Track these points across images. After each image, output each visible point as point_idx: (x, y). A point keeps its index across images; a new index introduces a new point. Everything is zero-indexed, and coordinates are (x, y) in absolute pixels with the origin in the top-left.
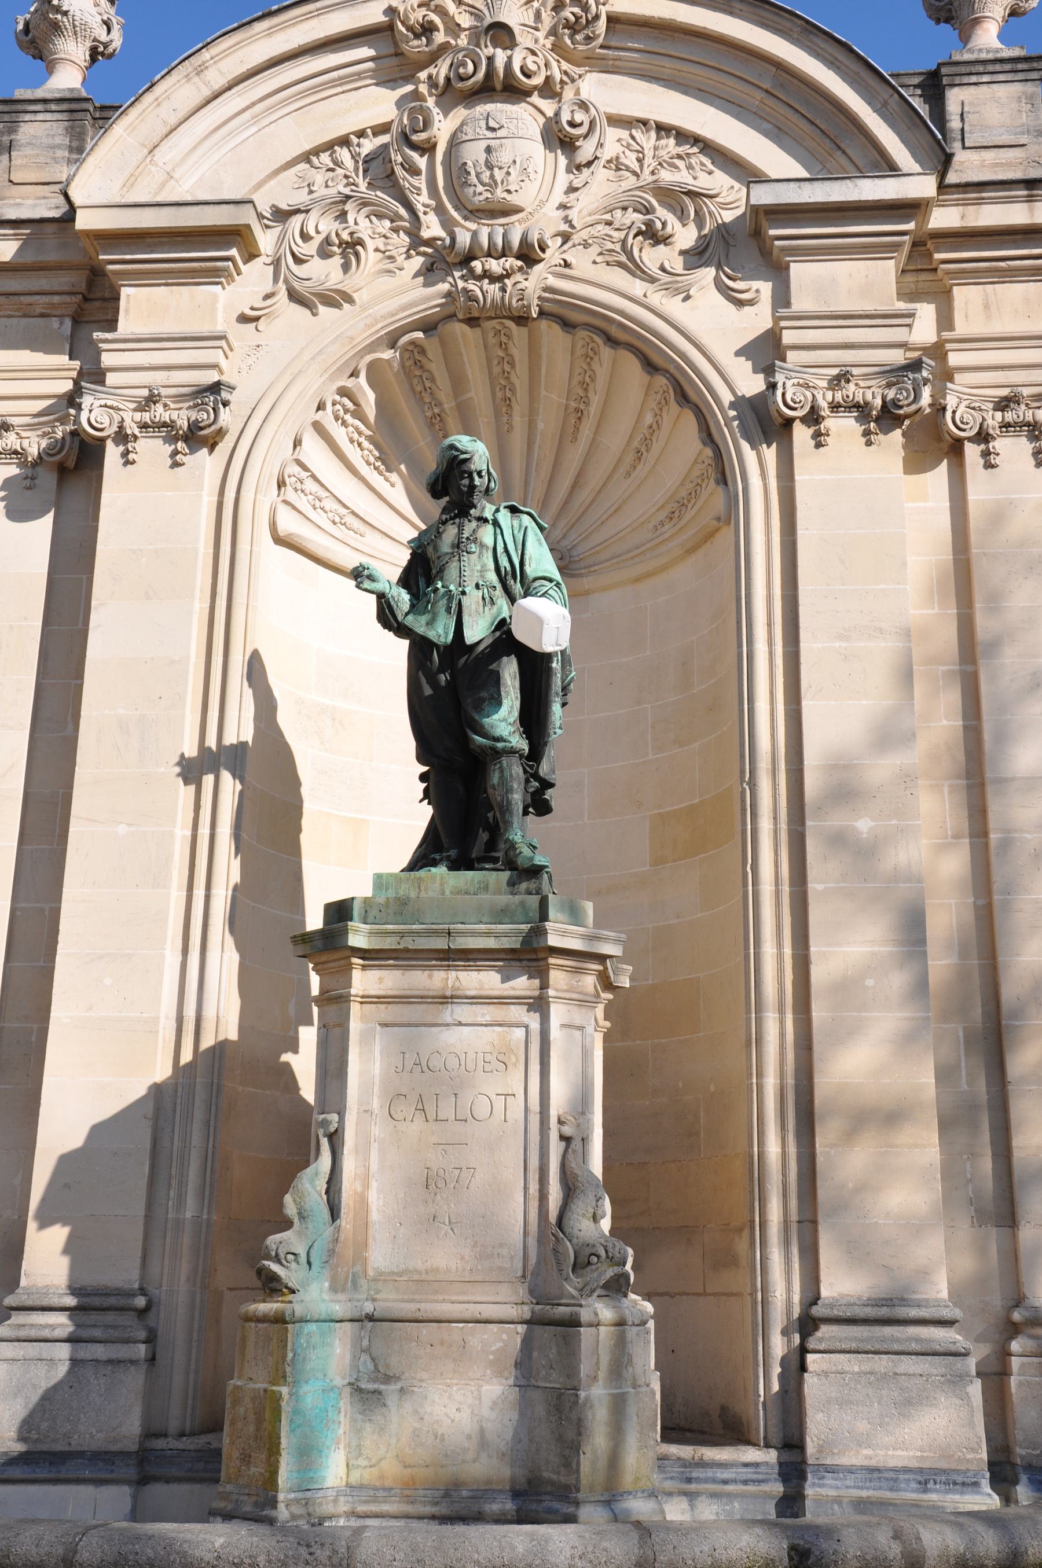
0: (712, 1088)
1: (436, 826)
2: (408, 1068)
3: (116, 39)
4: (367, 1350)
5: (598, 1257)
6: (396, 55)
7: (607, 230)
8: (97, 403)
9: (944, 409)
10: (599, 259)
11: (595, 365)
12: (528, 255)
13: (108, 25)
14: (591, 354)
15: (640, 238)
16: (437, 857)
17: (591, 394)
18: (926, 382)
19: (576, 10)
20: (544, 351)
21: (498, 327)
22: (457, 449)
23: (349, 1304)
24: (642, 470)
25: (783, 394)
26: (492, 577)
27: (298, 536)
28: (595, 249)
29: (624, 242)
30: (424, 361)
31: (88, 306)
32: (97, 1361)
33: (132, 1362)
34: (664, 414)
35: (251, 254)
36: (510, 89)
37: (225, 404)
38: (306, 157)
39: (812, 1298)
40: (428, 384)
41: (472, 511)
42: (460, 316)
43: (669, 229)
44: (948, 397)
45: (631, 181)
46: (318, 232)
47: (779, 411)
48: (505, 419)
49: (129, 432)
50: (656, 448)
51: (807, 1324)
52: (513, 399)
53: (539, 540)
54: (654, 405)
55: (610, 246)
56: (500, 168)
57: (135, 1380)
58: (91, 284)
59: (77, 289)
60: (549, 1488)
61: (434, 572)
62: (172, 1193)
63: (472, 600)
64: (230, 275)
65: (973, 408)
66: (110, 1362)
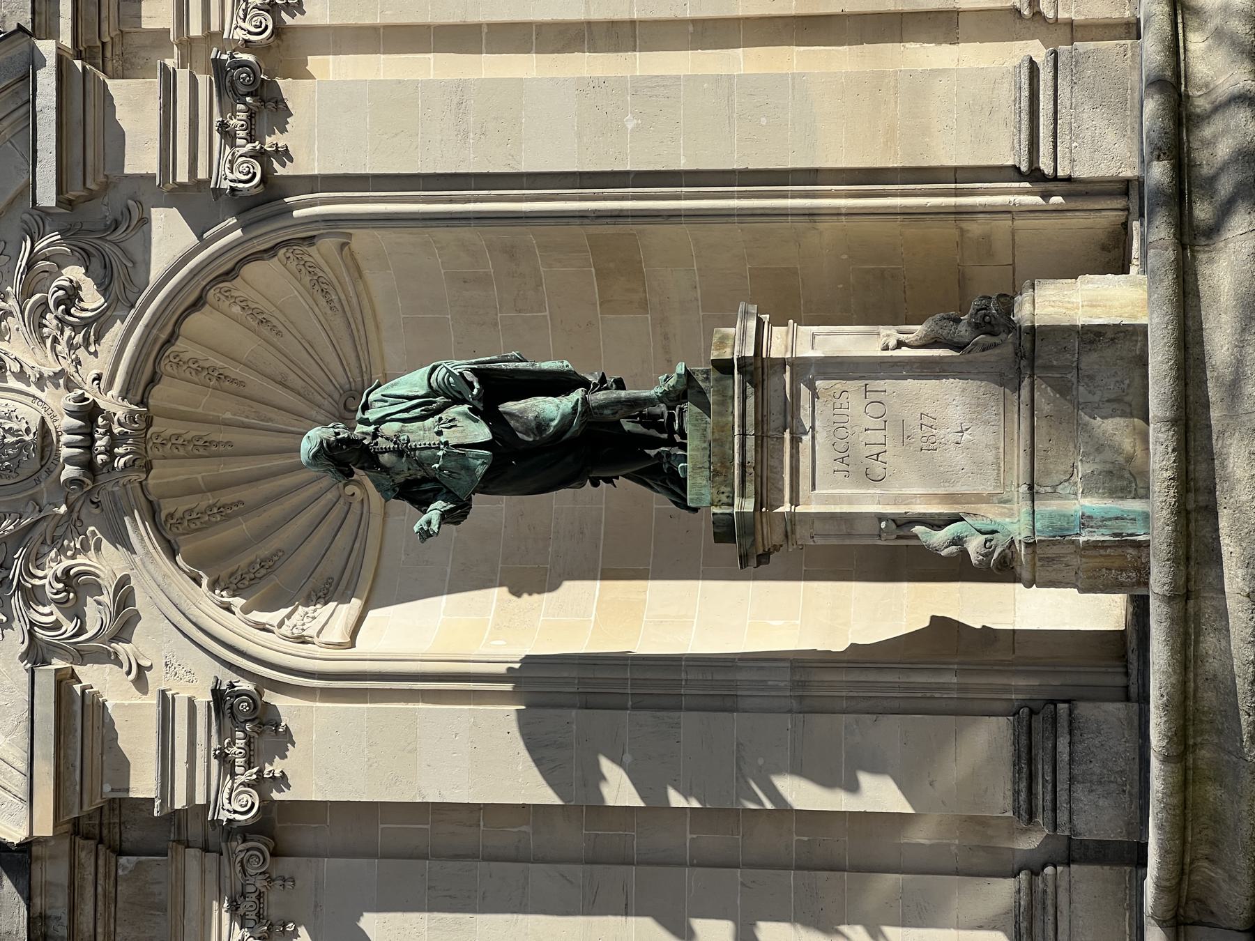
0: (845, 257)
1: (635, 472)
2: (844, 467)
4: (1054, 487)
5: (985, 315)
7: (63, 341)
8: (227, 806)
9: (246, 41)
10: (92, 349)
11: (186, 357)
12: (89, 413)
15: (73, 311)
18: (232, 57)
25: (240, 181)
26: (430, 422)
28: (81, 353)
30: (177, 515)
31: (106, 841)
35: (74, 677)
37: (232, 686)
40: (194, 516)
43: (67, 284)
44: (236, 37)
46: (51, 614)
47: (256, 186)
48: (222, 448)
49: (254, 777)
50: (263, 304)
51: (1034, 175)
52: (205, 439)
53: (392, 386)
56: (4, 437)
57: (1083, 709)
59: (94, 847)
62: (937, 695)
63: (452, 437)
65: (245, 16)
66: (1071, 733)
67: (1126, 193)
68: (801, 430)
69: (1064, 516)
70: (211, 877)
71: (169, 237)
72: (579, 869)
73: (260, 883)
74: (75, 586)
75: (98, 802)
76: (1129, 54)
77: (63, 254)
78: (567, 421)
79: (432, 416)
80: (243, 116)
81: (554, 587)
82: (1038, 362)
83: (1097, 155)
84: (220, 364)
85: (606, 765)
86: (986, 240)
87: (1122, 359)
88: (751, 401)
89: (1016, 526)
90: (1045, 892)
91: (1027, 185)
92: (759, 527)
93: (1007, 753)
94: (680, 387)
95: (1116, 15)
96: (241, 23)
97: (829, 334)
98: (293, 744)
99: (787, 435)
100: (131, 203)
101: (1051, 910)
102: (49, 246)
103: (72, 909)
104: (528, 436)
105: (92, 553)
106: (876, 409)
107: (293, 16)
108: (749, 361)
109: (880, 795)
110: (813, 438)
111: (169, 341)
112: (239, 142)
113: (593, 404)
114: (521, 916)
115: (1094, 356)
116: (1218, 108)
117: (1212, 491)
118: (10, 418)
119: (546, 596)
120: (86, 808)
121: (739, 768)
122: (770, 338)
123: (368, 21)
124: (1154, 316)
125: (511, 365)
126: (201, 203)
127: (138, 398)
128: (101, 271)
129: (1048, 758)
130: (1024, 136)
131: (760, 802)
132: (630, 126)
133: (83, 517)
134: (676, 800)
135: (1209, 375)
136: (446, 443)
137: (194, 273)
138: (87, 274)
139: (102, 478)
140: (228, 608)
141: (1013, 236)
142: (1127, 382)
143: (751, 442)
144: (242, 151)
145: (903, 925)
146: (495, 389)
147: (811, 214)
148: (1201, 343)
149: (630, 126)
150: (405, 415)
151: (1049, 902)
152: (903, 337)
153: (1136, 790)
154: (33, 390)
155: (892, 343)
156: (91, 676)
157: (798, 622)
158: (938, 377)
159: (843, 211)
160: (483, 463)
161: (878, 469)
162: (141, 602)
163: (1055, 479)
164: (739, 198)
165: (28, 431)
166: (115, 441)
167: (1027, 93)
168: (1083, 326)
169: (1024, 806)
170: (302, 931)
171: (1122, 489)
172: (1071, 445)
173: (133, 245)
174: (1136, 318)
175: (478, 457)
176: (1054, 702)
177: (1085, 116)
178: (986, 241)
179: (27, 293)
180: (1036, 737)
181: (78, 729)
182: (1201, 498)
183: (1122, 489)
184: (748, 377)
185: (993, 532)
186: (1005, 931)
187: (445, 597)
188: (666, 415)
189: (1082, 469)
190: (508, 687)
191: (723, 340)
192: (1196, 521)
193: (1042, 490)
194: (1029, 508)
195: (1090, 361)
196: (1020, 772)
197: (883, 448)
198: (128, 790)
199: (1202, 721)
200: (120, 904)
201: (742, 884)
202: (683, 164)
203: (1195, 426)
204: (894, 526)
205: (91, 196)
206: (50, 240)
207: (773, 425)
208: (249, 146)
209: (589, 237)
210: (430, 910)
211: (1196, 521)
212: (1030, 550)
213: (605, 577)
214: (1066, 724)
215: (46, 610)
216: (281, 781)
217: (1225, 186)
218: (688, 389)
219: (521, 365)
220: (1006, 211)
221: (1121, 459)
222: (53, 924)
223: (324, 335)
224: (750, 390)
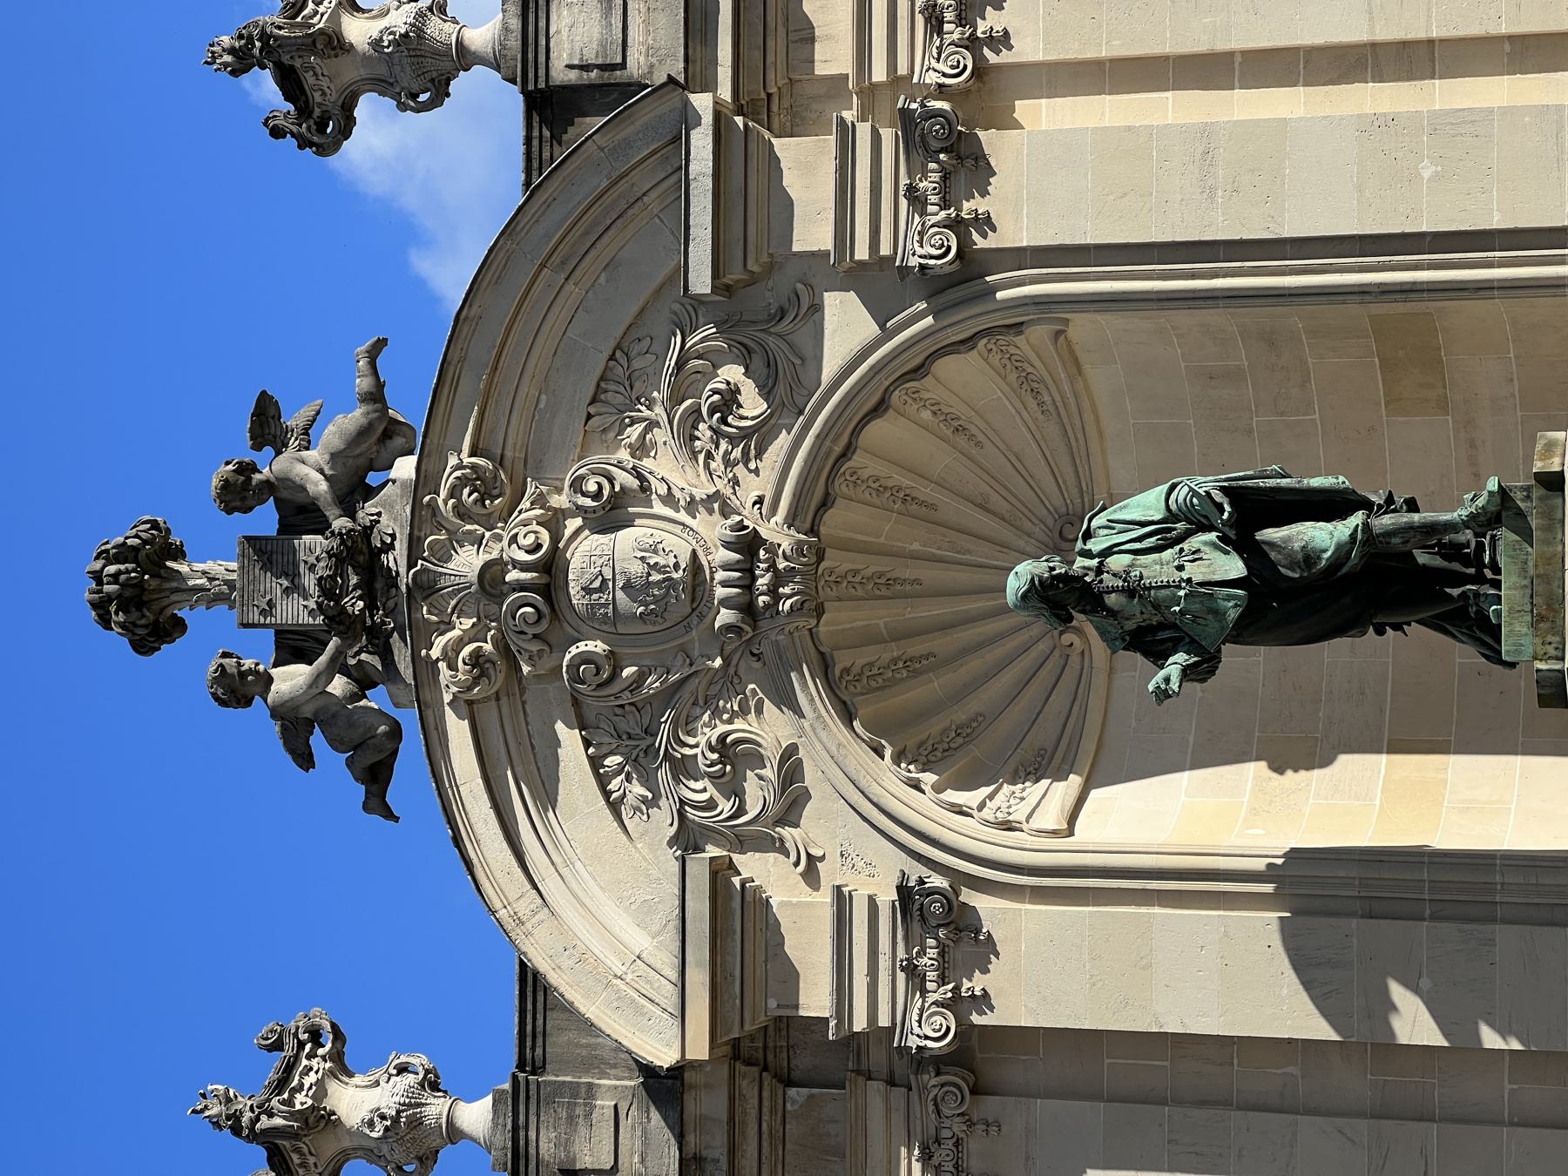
3: (419, 1060)
6: (498, 699)
8: (917, 1030)
9: (940, 86)
10: (752, 466)
12: (748, 545)
13: (402, 1069)
15: (730, 419)
17: (890, 483)
19: (466, 491)
25: (932, 257)
26: (1168, 554)
27: (1063, 806)
28: (740, 470)
31: (771, 1065)
36: (551, 567)
37: (921, 882)
38: (615, 807)
40: (875, 671)
43: (723, 386)
46: (705, 790)
47: (951, 263)
48: (908, 587)
56: (649, 574)
59: (757, 1075)
63: (1195, 572)
65: (939, 54)
70: (898, 1118)
71: (846, 326)
72: (1363, 1125)
73: (958, 1127)
74: (734, 758)
77: (719, 350)
78: (1343, 551)
80: (935, 177)
81: (1326, 762)
85: (1398, 992)
94: (1492, 508)
96: (934, 64)
98: (997, 955)
100: (800, 286)
102: (702, 340)
104: (1293, 571)
105: (752, 717)
107: (998, 52)
112: (930, 209)
113: (1376, 530)
118: (655, 552)
119: (1316, 772)
120: (747, 1027)
123: (1090, 54)
125: (1271, 483)
126: (882, 284)
127: (807, 525)
132: (1426, 174)
133: (741, 672)
134: (1491, 1039)
136: (1189, 581)
137: (876, 370)
139: (764, 625)
140: (916, 785)
144: (934, 219)
146: (1249, 512)
149: (1426, 174)
150: (1137, 546)
154: (682, 516)
160: (1236, 605)
165: (676, 566)
166: (779, 579)
173: (802, 338)
175: (1229, 598)
179: (675, 399)
187: (1187, 773)
188: (1473, 545)
190: (1268, 888)
198: (797, 1007)
200: (788, 1146)
202: (1497, 221)
205: (753, 280)
206: (704, 335)
208: (943, 214)
213: (1393, 749)
215: (699, 785)
216: (983, 1001)
219: (1284, 482)
223: (1034, 446)
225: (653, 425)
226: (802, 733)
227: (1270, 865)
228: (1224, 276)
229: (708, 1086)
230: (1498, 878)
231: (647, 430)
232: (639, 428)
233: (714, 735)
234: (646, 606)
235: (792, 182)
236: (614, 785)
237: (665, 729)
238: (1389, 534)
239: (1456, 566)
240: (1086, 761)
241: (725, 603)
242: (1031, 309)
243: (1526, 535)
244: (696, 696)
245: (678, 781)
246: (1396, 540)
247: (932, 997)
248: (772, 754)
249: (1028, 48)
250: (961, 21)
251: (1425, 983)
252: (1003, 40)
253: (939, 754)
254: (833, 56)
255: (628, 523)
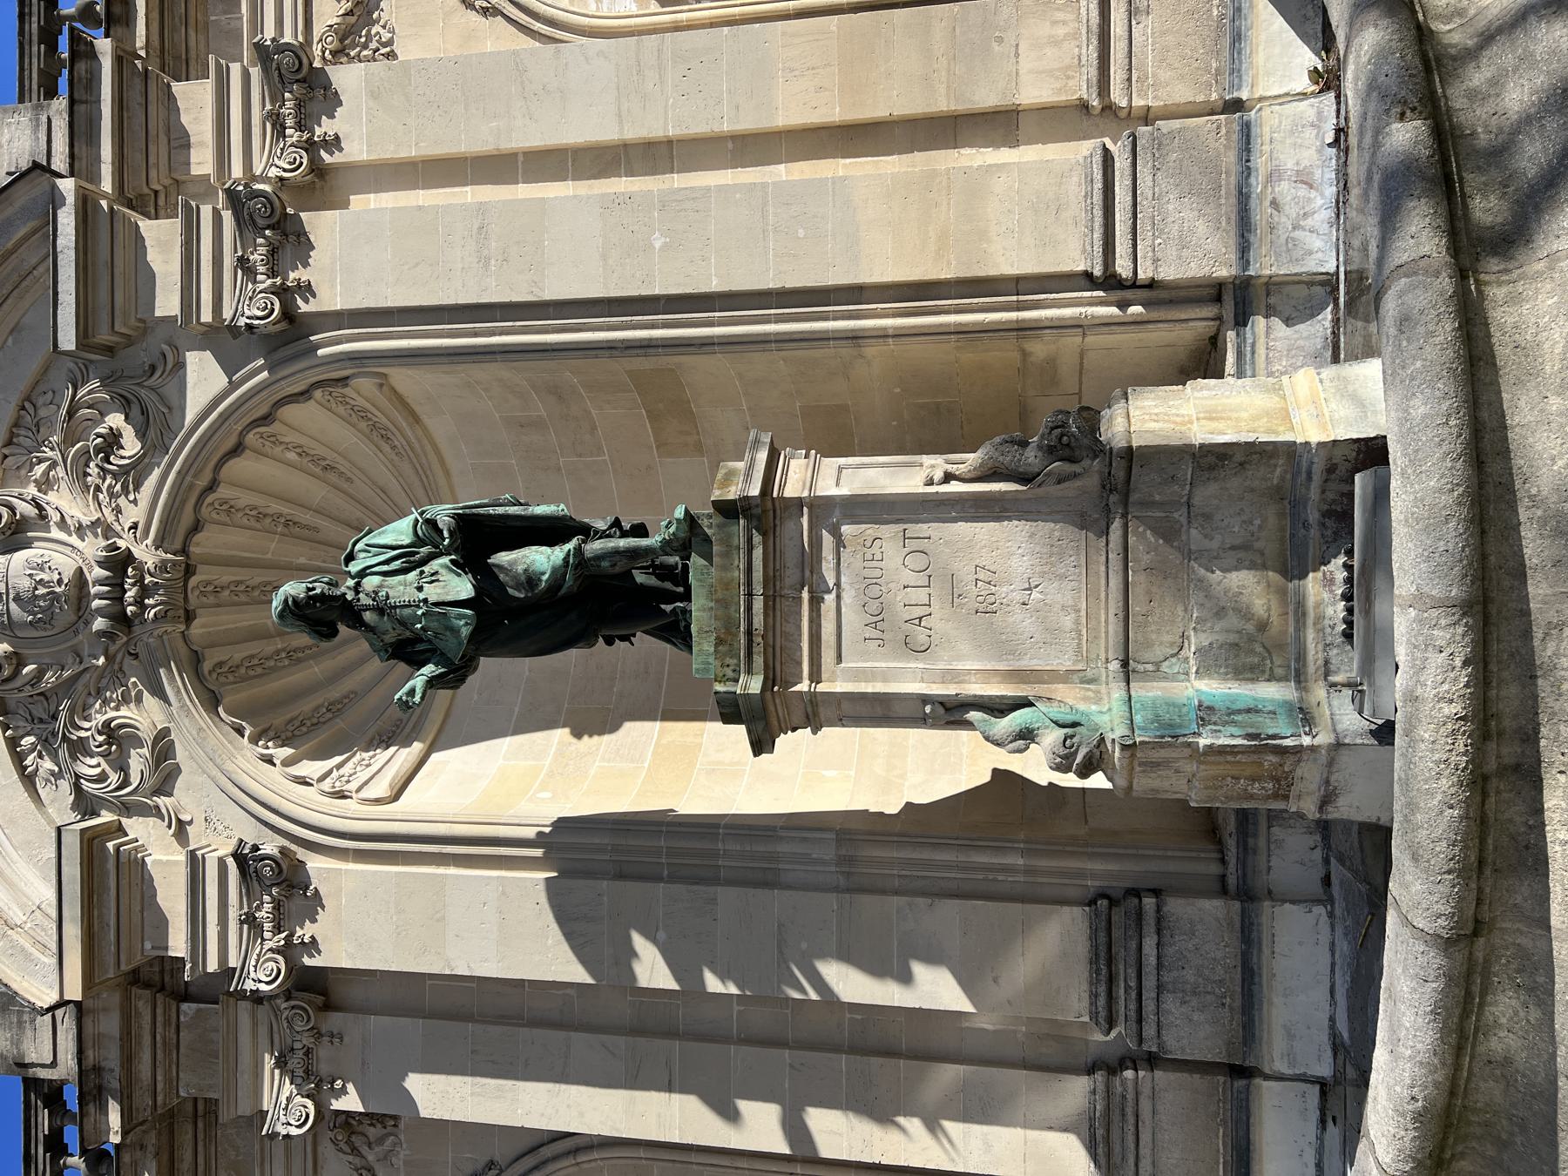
4: (1158, 664)
5: (1062, 435)
9: (281, 179)
10: (131, 497)
12: (119, 563)
14: (225, 507)
16: (683, 624)
17: (269, 511)
20: (224, 552)
21: (197, 593)
22: (283, 611)
23: (1112, 685)
24: (343, 466)
26: (413, 575)
28: (122, 501)
29: (115, 476)
31: (168, 987)
32: (1158, 944)
33: (1158, 910)
34: (286, 440)
37: (255, 848)
38: (28, 780)
39: (1088, 281)
40: (256, 661)
41: (349, 597)
42: (183, 627)
45: (60, 471)
50: (321, 451)
51: (1110, 282)
54: (278, 449)
55: (118, 487)
57: (1176, 906)
58: (147, 985)
60: (1289, 476)
61: (408, 634)
63: (433, 593)
64: (136, 849)
66: (1159, 932)
67: (1218, 299)
68: (823, 587)
69: (1174, 705)
70: (263, 1031)
71: (203, 379)
72: (621, 1041)
73: (307, 1040)
74: (117, 739)
75: (138, 960)
76: (1223, 131)
77: (104, 401)
79: (414, 569)
80: (263, 250)
81: (614, 728)
82: (1134, 497)
83: (1185, 253)
84: (286, 511)
85: (639, 942)
86: (1051, 363)
87: (1252, 490)
88: (758, 553)
89: (1106, 718)
90: (1124, 1097)
91: (1101, 293)
92: (772, 708)
93: (1082, 948)
95: (1201, 98)
96: (277, 161)
97: (859, 467)
98: (323, 908)
99: (805, 595)
100: (164, 347)
101: (1131, 1119)
102: (89, 393)
103: (128, 1059)
105: (132, 705)
106: (917, 561)
107: (331, 154)
108: (753, 503)
109: (936, 989)
110: (839, 597)
111: (212, 487)
112: (260, 277)
113: (588, 554)
114: (564, 1087)
115: (1212, 488)
116: (1488, 38)
117: (1530, 737)
118: (42, 570)
119: (606, 738)
120: (123, 967)
121: (781, 952)
122: (785, 472)
123: (403, 153)
124: (1416, 402)
125: (500, 510)
126: (229, 342)
127: (178, 545)
128: (140, 418)
129: (1132, 960)
130: (1098, 235)
131: (804, 991)
132: (657, 245)
133: (125, 668)
134: (713, 984)
135: (1523, 515)
136: (425, 601)
137: (224, 417)
138: (127, 419)
139: (137, 630)
140: (269, 760)
141: (1082, 359)
142: (1258, 522)
143: (758, 604)
144: (262, 286)
145: (965, 1120)
146: (477, 539)
147: (855, 337)
148: (1505, 453)
149: (657, 245)
150: (385, 568)
151: (1129, 1111)
152: (951, 468)
153: (1238, 1003)
154: (74, 540)
155: (938, 475)
156: (136, 827)
157: (852, 773)
158: (998, 519)
159: (891, 332)
161: (921, 636)
162: (181, 755)
163: (1159, 652)
164: (776, 322)
165: (60, 582)
166: (145, 591)
167: (1100, 185)
168: (1202, 446)
169: (1103, 1014)
170: (350, 1087)
171: (1252, 668)
172: (1180, 610)
173: (170, 390)
174: (1276, 433)
176: (1136, 893)
177: (1171, 207)
178: (1050, 367)
179: (69, 441)
180: (1116, 933)
181: (105, 884)
182: (1505, 751)
183: (1252, 668)
184: (755, 523)
185: (1075, 725)
186: (1078, 1135)
189: (1194, 642)
190: (538, 852)
191: (731, 474)
192: (1498, 792)
193: (1140, 667)
194: (1124, 693)
195: (1206, 494)
196: (1098, 972)
197: (926, 610)
198: (167, 948)
199: (1469, 1123)
200: (182, 1050)
201: (791, 1066)
202: (715, 285)
203: (1499, 612)
204: (941, 710)
205: (130, 341)
206: (91, 389)
207: (788, 581)
208: (269, 282)
209: (630, 373)
210: (473, 1074)
211: (1498, 792)
212: (1127, 754)
213: (665, 718)
214: (1152, 922)
215: (94, 761)
216: (313, 946)
217: (1533, 155)
218: (691, 537)
219: (512, 510)
220: (1077, 325)
221: (1250, 627)
222: (107, 1076)
224: (757, 538)
225: (54, 465)
226: (171, 717)
227: (540, 834)
228: (501, 334)
229: (105, 1010)
230: (720, 846)
231: (50, 468)
232: (44, 466)
233: (101, 719)
234: (34, 614)
235: (153, 257)
236: (28, 762)
237: (62, 716)
238: (599, 557)
239: (668, 585)
240: (431, 731)
241: (100, 612)
242: (348, 363)
243: (708, 557)
244: (87, 689)
245: (74, 758)
246: (605, 564)
247: (268, 945)
248: (147, 734)
249: (355, 150)
250: (300, 127)
251: (661, 935)
252: (334, 143)
253: (304, 729)
254: (202, 162)
255: (27, 545)
